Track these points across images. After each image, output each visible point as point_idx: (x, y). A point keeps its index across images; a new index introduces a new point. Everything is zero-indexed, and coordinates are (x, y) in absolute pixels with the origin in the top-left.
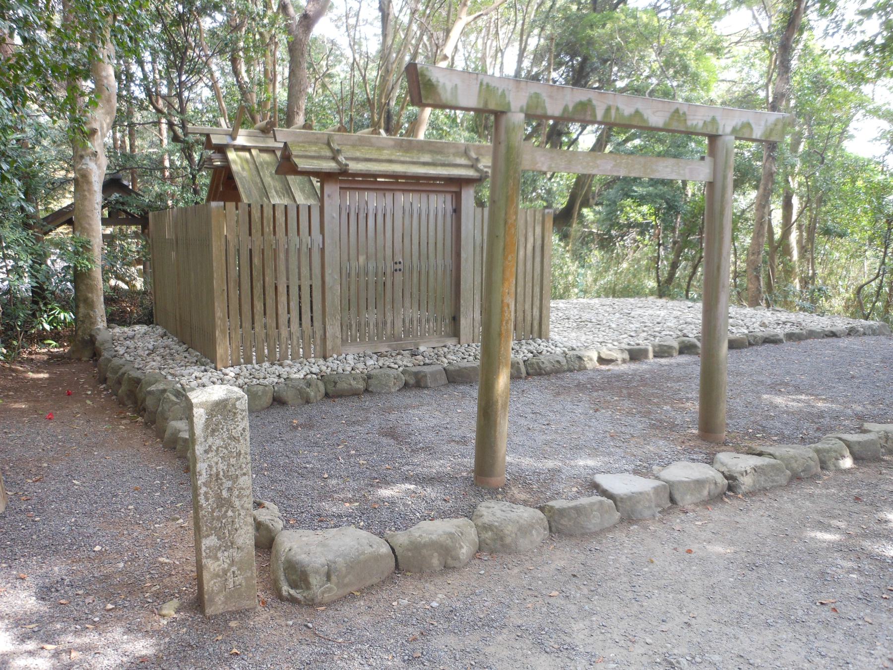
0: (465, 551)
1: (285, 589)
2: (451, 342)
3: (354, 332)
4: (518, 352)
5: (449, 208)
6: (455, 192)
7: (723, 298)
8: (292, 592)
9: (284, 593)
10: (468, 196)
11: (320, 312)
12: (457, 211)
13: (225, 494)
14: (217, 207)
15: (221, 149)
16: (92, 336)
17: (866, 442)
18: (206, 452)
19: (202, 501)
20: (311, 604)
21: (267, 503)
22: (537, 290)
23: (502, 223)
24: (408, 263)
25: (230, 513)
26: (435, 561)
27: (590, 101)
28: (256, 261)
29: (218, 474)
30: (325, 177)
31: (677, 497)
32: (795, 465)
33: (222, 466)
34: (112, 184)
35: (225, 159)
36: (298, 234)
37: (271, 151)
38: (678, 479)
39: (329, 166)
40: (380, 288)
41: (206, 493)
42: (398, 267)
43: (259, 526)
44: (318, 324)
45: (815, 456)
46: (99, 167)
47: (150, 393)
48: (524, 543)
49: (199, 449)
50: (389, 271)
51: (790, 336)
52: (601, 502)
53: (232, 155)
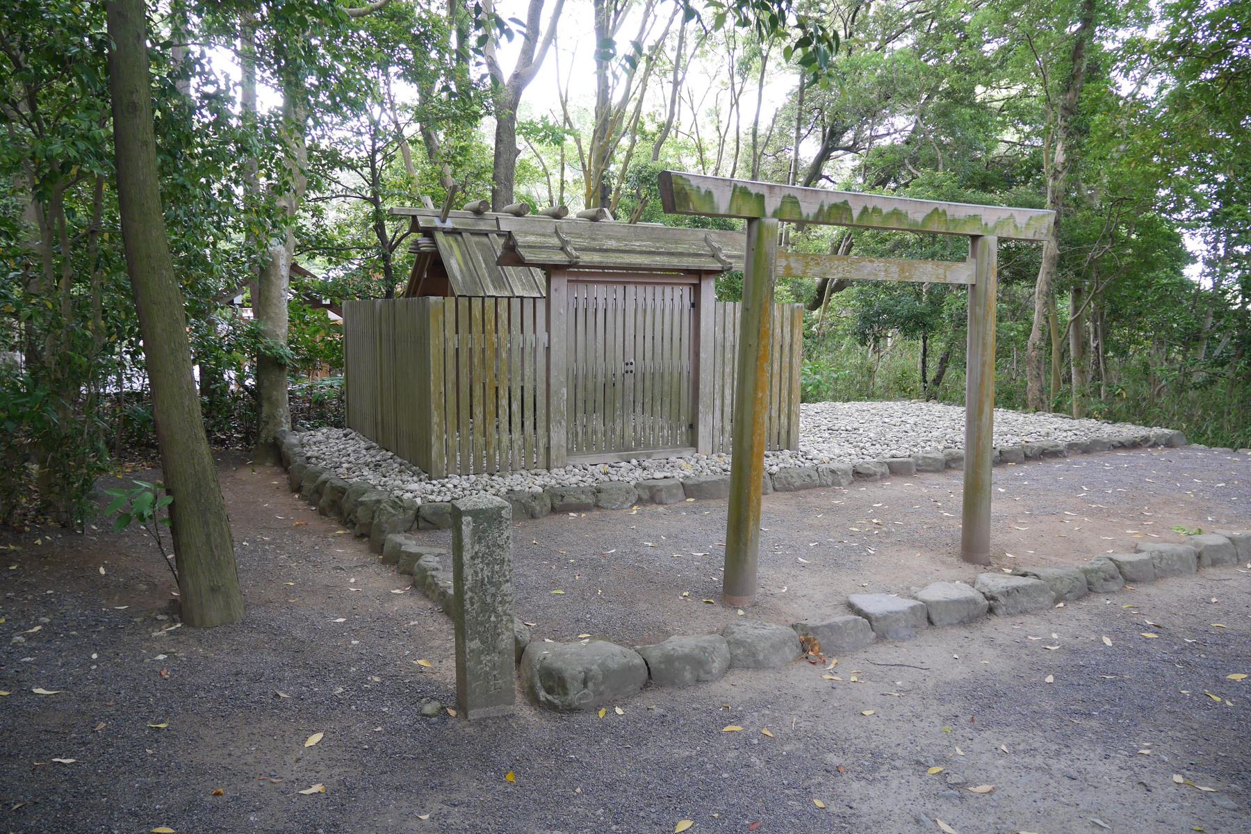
0: (716, 666)
1: (543, 695)
2: (687, 453)
4: (774, 462)
5: (687, 303)
6: (694, 285)
7: (988, 403)
8: (550, 697)
9: (542, 699)
10: (709, 290)
11: (544, 418)
12: (696, 305)
13: (489, 600)
14: (436, 302)
15: (429, 233)
16: (275, 438)
17: (1140, 561)
18: (473, 558)
20: (571, 710)
23: (755, 332)
25: (493, 619)
26: (688, 675)
27: (846, 203)
30: (551, 270)
31: (934, 618)
32: (1059, 585)
33: (487, 573)
35: (434, 242)
36: (535, 332)
38: (937, 599)
39: (559, 258)
41: (471, 598)
42: (630, 368)
44: (541, 431)
45: (1083, 576)
47: (362, 503)
48: (775, 660)
51: (1072, 447)
52: (855, 620)
53: (440, 237)
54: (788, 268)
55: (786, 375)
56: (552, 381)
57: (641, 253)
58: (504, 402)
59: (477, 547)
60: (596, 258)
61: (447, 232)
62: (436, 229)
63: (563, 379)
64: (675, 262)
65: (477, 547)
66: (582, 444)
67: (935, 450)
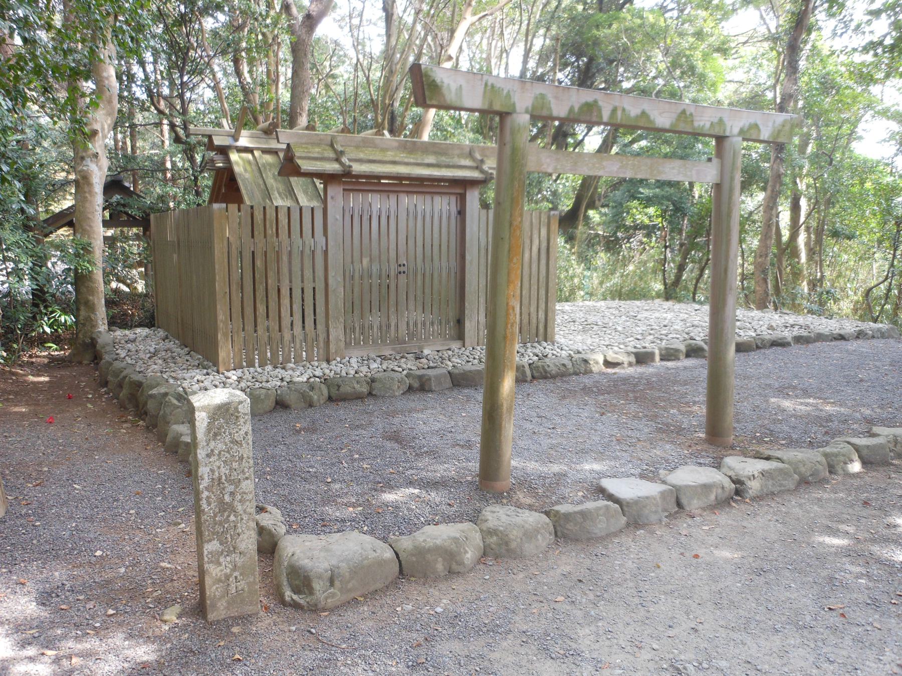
0: (470, 556)
1: (288, 594)
2: (455, 345)
4: (523, 355)
5: (454, 210)
6: (460, 194)
8: (295, 597)
9: (287, 599)
10: (473, 198)
11: (323, 315)
12: (462, 213)
13: (227, 498)
14: (219, 209)
15: (224, 151)
16: (93, 339)
17: (875, 446)
18: (208, 456)
19: (204, 506)
20: (314, 609)
21: (269, 508)
22: (542, 292)
23: (507, 225)
24: (412, 266)
25: (232, 518)
26: (440, 566)
27: (596, 101)
28: (259, 263)
29: (220, 479)
30: (329, 178)
31: (684, 501)
32: (803, 469)
33: (224, 470)
34: (113, 186)
35: (228, 160)
37: (274, 152)
38: (685, 483)
39: (332, 167)
40: (384, 291)
41: (208, 498)
42: (402, 269)
43: (261, 530)
44: (321, 327)
45: (824, 460)
46: (100, 169)
47: (151, 396)
48: (529, 548)
49: (201, 453)
50: (392, 274)
51: (798, 339)
52: (607, 507)
53: (234, 157)
66: (357, 335)
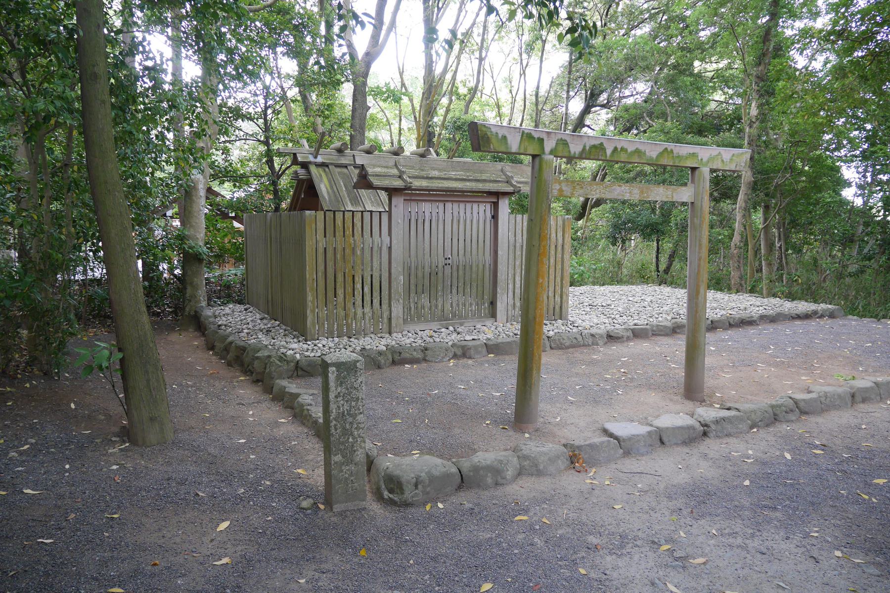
0: (510, 473)
1: (386, 494)
2: (489, 322)
3: (414, 316)
4: (551, 329)
5: (489, 215)
6: (494, 202)
8: (391, 496)
9: (386, 497)
10: (504, 206)
11: (387, 297)
12: (495, 217)
13: (348, 426)
14: (310, 215)
15: (305, 165)
16: (196, 312)
18: (336, 397)
20: (407, 505)
23: (537, 236)
25: (351, 440)
26: (489, 480)
27: (602, 144)
30: (392, 192)
31: (665, 439)
32: (753, 416)
33: (346, 407)
35: (309, 172)
38: (666, 426)
39: (398, 183)
41: (335, 425)
42: (448, 261)
44: (385, 306)
45: (770, 410)
47: (257, 358)
48: (552, 469)
52: (609, 441)
53: (313, 169)
54: (561, 190)
55: (559, 267)
56: (393, 271)
57: (456, 180)
58: (359, 286)
59: (339, 389)
60: (424, 183)
61: (318, 165)
62: (310, 163)
63: (400, 269)
64: (480, 186)
65: (339, 389)
67: (665, 320)
